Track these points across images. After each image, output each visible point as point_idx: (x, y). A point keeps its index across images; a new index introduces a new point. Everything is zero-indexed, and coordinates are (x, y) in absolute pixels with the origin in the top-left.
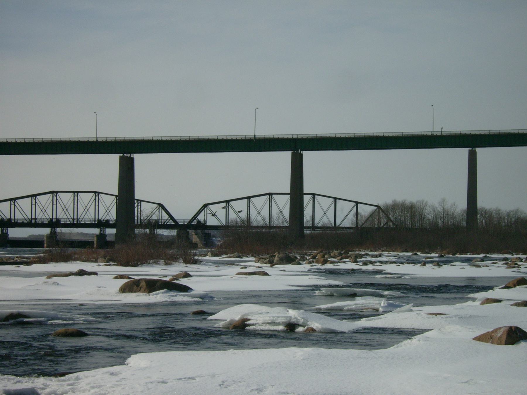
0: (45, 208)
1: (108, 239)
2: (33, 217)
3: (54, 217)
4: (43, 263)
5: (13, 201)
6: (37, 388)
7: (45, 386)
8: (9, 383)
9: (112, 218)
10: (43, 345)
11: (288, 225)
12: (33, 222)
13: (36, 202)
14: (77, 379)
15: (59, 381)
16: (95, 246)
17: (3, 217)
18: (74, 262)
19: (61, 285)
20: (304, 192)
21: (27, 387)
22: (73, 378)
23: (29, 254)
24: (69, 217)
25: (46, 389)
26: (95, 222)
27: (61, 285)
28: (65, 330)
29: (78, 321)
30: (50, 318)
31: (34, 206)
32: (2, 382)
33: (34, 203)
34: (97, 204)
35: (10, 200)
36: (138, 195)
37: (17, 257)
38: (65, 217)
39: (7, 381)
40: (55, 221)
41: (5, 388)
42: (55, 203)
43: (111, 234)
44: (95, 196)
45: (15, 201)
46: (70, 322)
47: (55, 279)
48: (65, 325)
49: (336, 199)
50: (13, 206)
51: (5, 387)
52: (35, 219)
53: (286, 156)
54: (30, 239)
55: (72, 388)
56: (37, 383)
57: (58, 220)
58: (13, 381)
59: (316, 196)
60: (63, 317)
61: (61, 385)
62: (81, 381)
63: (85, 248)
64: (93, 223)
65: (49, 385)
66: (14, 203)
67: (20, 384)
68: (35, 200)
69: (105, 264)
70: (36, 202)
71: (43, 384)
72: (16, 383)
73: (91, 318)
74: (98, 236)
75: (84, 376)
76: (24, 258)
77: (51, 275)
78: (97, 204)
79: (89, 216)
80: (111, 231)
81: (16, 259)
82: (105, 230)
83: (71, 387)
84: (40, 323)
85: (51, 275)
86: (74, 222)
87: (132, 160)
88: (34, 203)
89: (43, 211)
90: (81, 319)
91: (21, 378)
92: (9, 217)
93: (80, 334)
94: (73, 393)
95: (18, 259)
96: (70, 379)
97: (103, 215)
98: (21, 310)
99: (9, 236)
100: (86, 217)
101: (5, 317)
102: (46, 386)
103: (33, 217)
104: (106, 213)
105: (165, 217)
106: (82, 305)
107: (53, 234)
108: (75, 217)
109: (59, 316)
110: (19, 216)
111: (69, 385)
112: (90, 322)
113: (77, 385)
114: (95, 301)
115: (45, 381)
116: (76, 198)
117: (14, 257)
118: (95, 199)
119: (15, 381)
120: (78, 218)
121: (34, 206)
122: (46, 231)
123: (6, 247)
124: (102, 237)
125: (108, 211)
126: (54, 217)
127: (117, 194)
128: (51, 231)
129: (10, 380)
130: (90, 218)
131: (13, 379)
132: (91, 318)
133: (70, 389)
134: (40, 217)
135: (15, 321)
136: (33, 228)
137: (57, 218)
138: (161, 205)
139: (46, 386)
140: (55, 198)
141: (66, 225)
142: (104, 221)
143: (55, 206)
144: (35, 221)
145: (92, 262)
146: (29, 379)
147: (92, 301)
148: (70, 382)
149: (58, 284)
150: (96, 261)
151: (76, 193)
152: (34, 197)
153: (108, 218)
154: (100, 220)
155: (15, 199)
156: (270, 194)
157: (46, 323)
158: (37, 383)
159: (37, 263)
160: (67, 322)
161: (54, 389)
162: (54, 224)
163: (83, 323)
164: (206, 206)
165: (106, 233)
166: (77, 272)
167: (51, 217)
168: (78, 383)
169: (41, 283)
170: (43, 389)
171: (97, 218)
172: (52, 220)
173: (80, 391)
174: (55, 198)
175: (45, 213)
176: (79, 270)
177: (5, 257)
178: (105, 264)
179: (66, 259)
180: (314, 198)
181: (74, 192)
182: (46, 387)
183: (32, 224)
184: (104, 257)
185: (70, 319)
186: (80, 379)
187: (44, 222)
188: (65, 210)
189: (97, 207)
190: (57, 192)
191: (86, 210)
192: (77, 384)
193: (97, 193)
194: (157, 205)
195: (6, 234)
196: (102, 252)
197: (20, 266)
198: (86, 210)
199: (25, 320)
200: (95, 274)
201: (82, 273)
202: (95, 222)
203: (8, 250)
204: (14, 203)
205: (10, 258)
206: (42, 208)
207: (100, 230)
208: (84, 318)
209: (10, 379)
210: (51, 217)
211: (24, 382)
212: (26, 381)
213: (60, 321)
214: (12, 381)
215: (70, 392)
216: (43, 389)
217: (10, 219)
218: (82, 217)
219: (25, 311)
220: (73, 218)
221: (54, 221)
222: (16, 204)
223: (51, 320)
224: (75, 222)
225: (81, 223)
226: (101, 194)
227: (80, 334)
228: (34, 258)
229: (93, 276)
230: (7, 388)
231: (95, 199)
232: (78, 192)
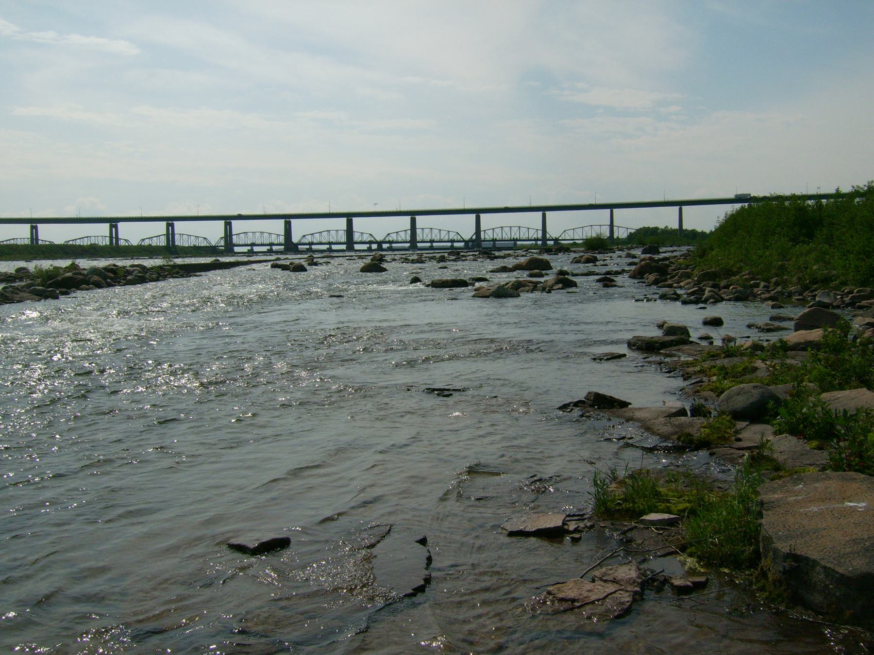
10: (167, 520)
36: (354, 230)
49: (440, 230)
53: (474, 216)
79: (446, 238)
80: (540, 243)
87: (415, 218)
105: (459, 237)
110: (315, 241)
127: (346, 229)
138: (371, 235)
151: (337, 231)
155: (313, 234)
156: (502, 227)
164: (389, 234)
180: (431, 232)
183: (321, 244)
195: (311, 248)
198: (427, 236)
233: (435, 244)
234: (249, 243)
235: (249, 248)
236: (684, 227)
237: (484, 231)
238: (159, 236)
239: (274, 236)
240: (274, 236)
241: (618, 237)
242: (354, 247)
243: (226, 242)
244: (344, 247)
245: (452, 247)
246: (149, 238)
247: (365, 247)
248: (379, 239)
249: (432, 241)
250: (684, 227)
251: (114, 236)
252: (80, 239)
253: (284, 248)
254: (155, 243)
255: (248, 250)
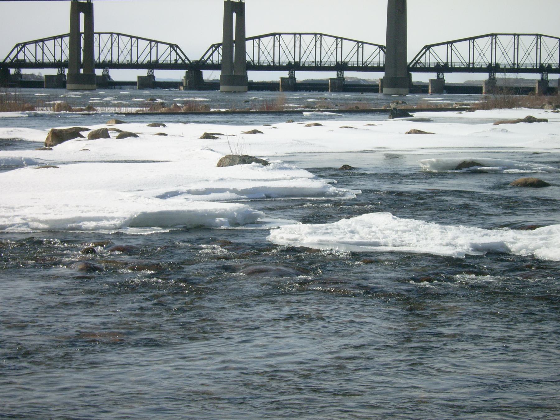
0: (484, 52)
1: (550, 85)
2: (471, 61)
3: (493, 61)
4: (486, 110)
5: (450, 44)
6: (507, 242)
7: (516, 240)
8: (475, 236)
9: (554, 62)
11: (411, 63)
12: (471, 66)
13: (474, 46)
14: (550, 232)
15: (530, 234)
16: (537, 92)
17: (440, 61)
18: (520, 108)
19: (511, 133)
20: (95, 31)
21: (496, 241)
22: (545, 232)
23: (467, 100)
24: (509, 62)
25: (517, 243)
26: (537, 66)
27: (511, 133)
28: (525, 179)
29: (535, 170)
30: (506, 167)
31: (471, 50)
32: (468, 234)
33: (472, 46)
34: (539, 47)
35: (447, 43)
37: (456, 104)
38: (505, 61)
39: (473, 234)
40: (383, 66)
41: (471, 241)
42: (494, 46)
43: (553, 80)
44: (537, 39)
45: (452, 44)
46: (528, 171)
47: (502, 126)
48: (522, 174)
50: (449, 50)
51: (471, 240)
52: (473, 63)
54: (466, 85)
55: (546, 243)
56: (506, 236)
57: (497, 65)
58: (479, 233)
59: (543, 37)
60: (520, 165)
61: (533, 239)
62: (555, 235)
63: (527, 94)
64: (535, 67)
65: (519, 239)
66: (451, 47)
67: (488, 237)
68: (474, 43)
69: (552, 110)
70: (474, 46)
71: (513, 238)
72: (483, 236)
73: (550, 167)
74: (539, 82)
75: (558, 230)
76: (463, 104)
77: (498, 122)
78: (539, 47)
79: (530, 61)
81: (454, 106)
82: (21, 71)
83: (544, 241)
84: (495, 172)
85: (498, 122)
86: (514, 66)
88: (472, 46)
89: (482, 54)
90: (540, 168)
91: (489, 231)
92: (446, 62)
93: (541, 184)
94: (547, 249)
95: (457, 105)
96: (542, 233)
97: (545, 60)
98: (474, 158)
99: (446, 82)
100: (527, 61)
101: (457, 165)
102: (516, 240)
103: (471, 61)
104: (549, 57)
106: (537, 153)
107: (492, 80)
108: (516, 62)
109: (516, 165)
110: (456, 61)
111: (542, 239)
112: (549, 172)
113: (551, 240)
114: (549, 150)
115: (515, 235)
116: (516, 40)
117: (453, 103)
118: (537, 42)
119: (482, 234)
120: (519, 62)
121: (471, 50)
122: (485, 76)
123: (442, 93)
124: (543, 82)
125: (550, 55)
126: (493, 61)
128: (490, 76)
129: (476, 233)
130: (532, 62)
131: (480, 232)
132: (550, 167)
133: (543, 243)
134: (478, 61)
135: (469, 169)
136: (471, 73)
137: (497, 62)
139: (516, 240)
140: (494, 41)
141: (353, 69)
142: (546, 66)
143: (494, 50)
144: (473, 66)
145: (538, 108)
146: (497, 232)
147: (546, 149)
148: (542, 236)
149: (507, 131)
150: (542, 108)
152: (472, 40)
153: (550, 62)
154: (542, 65)
155: (452, 42)
157: (502, 172)
158: (506, 236)
159: (480, 109)
160: (524, 171)
161: (526, 244)
162: (492, 68)
163: (541, 173)
165: (548, 79)
166: (523, 120)
167: (490, 62)
168: (552, 237)
169: (488, 130)
170: (513, 243)
171: (538, 62)
172: (490, 64)
173: (554, 246)
174: (494, 41)
175: (484, 57)
176: (527, 117)
177: (444, 104)
178: (552, 110)
179: (510, 105)
181: (514, 35)
182: (517, 241)
183: (470, 69)
184: (550, 103)
185: (527, 168)
186: (552, 233)
187: (483, 67)
188: (505, 54)
189: (539, 50)
190: (496, 35)
191: (527, 54)
192: (551, 238)
193: (539, 36)
194: (377, 47)
195: (443, 80)
196: (547, 98)
197: (462, 112)
198: (527, 54)
199: (479, 169)
200: (545, 121)
201: (530, 120)
202: (537, 66)
203: (445, 97)
204: (451, 47)
205: (449, 104)
206: (480, 52)
207: (542, 75)
208: (542, 168)
209: (477, 231)
210: (490, 62)
211: (492, 235)
212: (493, 234)
213: (517, 170)
214: (479, 234)
215: (544, 247)
216: (513, 243)
217: (446, 64)
218: (522, 62)
219: (478, 158)
220: (513, 62)
221: (493, 65)
222: (453, 48)
223: (507, 169)
224: (516, 67)
225: (522, 67)
226: (323, 36)
227: (541, 184)
228: (474, 104)
229: (543, 123)
230: (474, 242)
231: (537, 42)
232: (518, 35)
233: (348, 75)
234: (285, 60)
235: (144, 73)
236: (69, 32)
237: (99, 34)
238: (259, 37)
239: (348, 46)
240: (348, 46)
241: (104, 61)
242: (246, 77)
243: (227, 54)
244: (377, 77)
245: (341, 78)
246: (36, 42)
247: (132, 75)
248: (194, 56)
249: (341, 67)
250: (69, 32)
251: (82, 30)
252: (55, 38)
253: (187, 77)
254: (508, 67)
255: (283, 79)
